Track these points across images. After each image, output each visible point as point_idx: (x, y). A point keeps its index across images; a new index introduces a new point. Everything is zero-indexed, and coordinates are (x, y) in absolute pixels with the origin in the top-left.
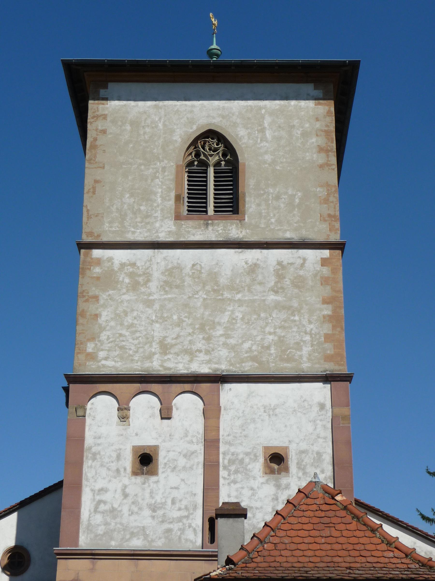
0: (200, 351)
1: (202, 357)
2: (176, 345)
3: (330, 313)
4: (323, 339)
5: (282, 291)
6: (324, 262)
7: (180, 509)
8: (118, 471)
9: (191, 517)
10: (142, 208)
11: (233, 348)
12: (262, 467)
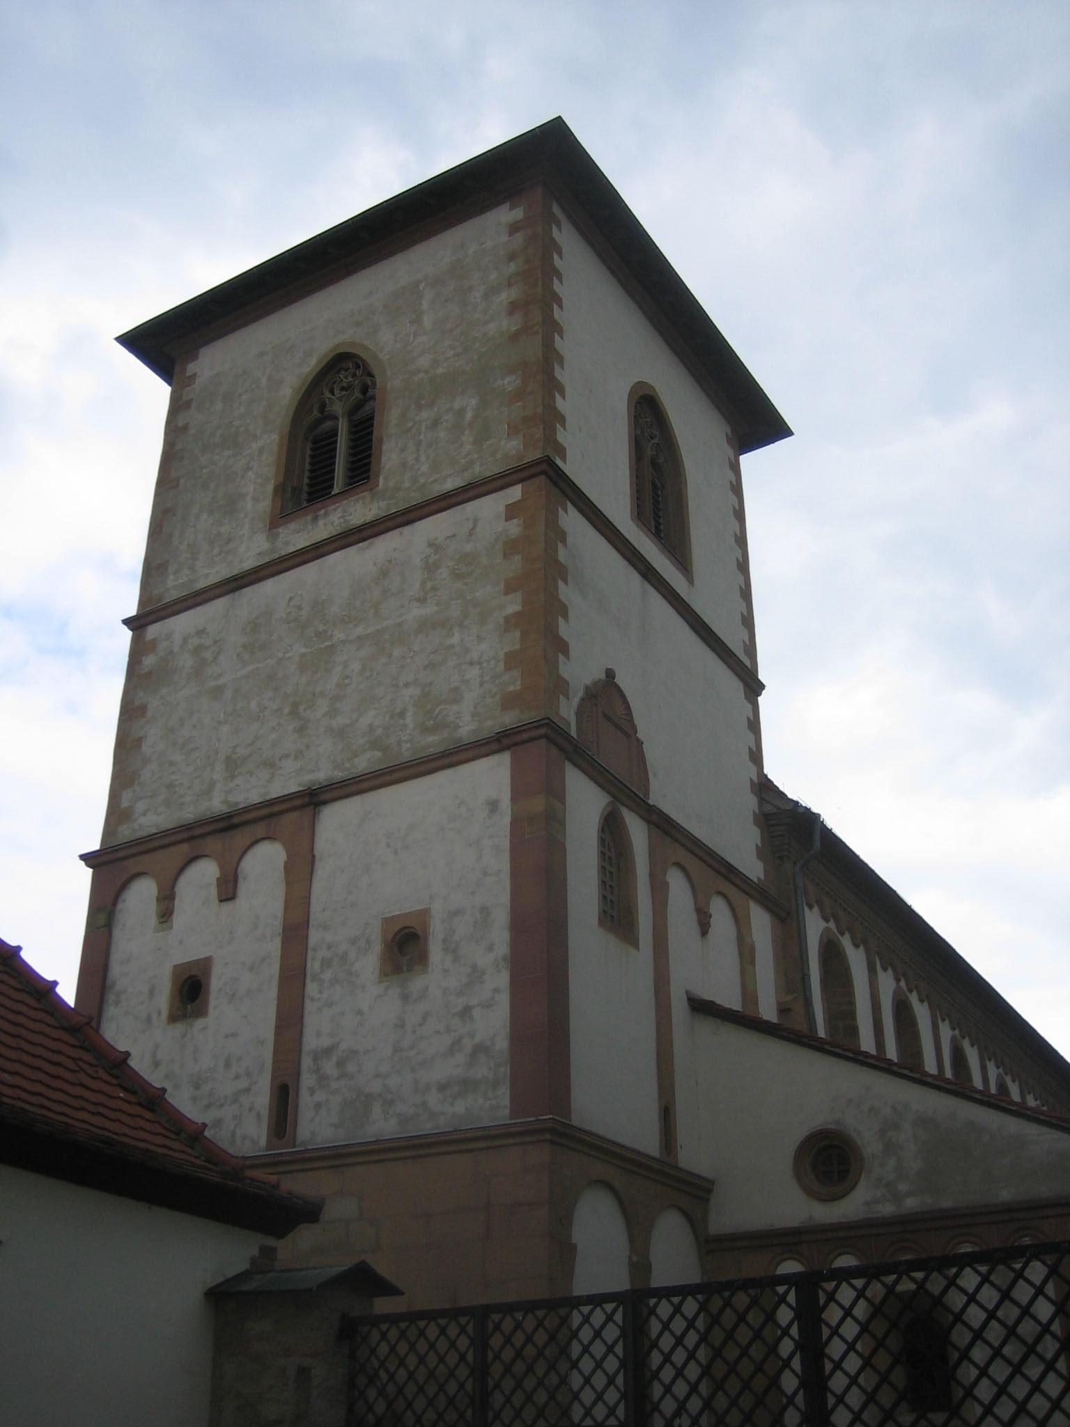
0: (287, 756)
1: (290, 765)
2: (251, 755)
3: (517, 608)
4: (501, 665)
5: (432, 594)
6: (511, 511)
7: (237, 1077)
8: (149, 1019)
10: (223, 530)
11: (341, 733)
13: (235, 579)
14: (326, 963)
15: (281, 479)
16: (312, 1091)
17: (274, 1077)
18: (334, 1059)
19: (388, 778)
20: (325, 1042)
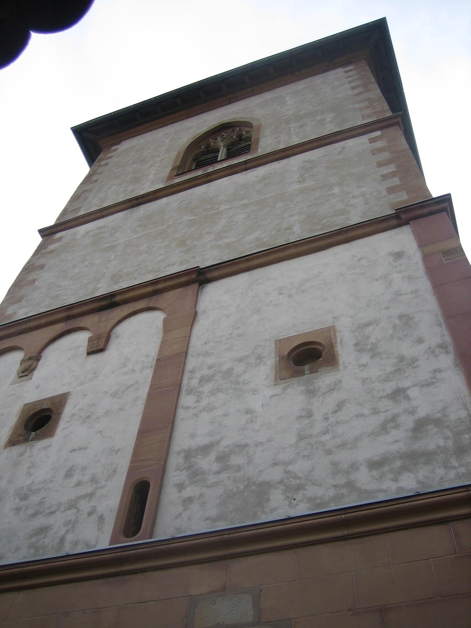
9: (99, 493)
12: (274, 370)
13: (137, 198)
14: (203, 380)
15: (178, 164)
16: (180, 487)
17: (131, 470)
18: (213, 456)
19: (281, 255)
20: (201, 441)
